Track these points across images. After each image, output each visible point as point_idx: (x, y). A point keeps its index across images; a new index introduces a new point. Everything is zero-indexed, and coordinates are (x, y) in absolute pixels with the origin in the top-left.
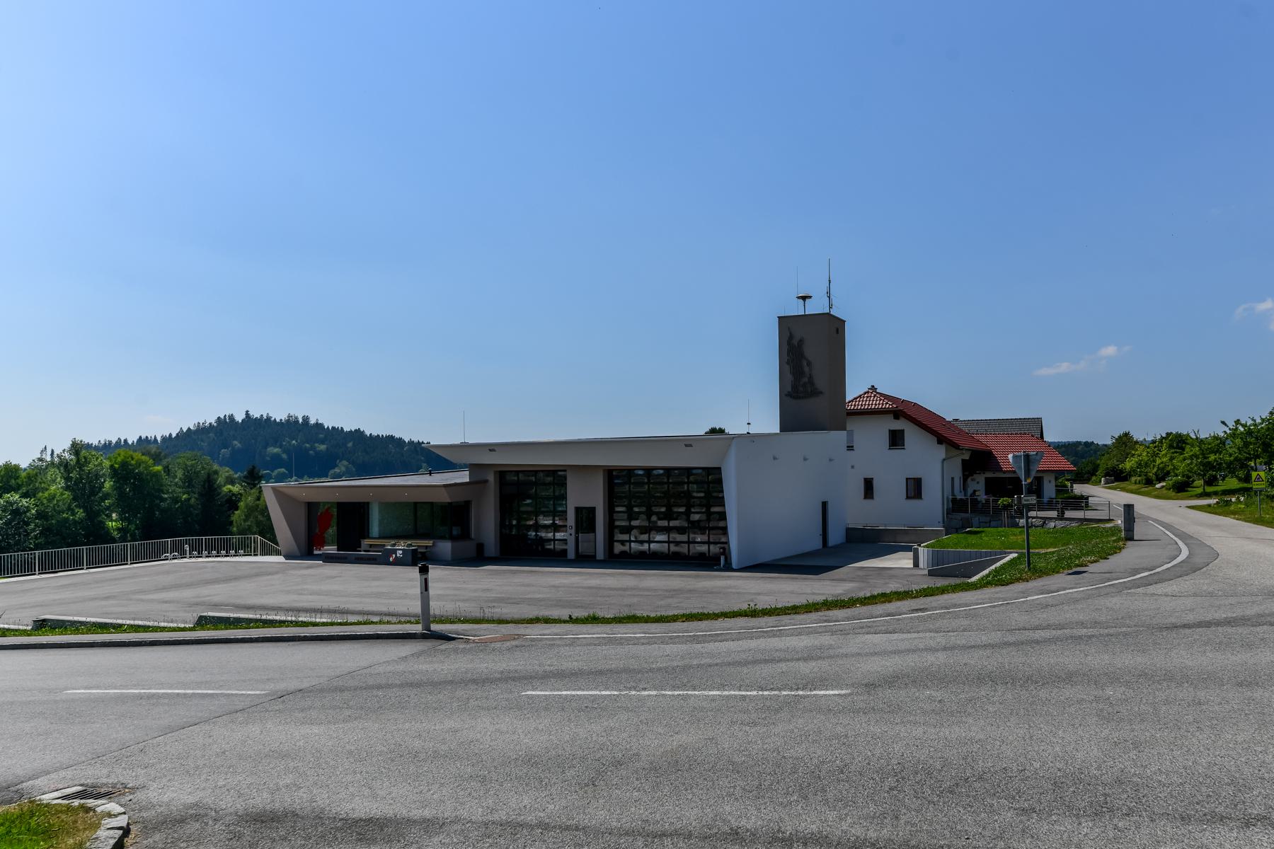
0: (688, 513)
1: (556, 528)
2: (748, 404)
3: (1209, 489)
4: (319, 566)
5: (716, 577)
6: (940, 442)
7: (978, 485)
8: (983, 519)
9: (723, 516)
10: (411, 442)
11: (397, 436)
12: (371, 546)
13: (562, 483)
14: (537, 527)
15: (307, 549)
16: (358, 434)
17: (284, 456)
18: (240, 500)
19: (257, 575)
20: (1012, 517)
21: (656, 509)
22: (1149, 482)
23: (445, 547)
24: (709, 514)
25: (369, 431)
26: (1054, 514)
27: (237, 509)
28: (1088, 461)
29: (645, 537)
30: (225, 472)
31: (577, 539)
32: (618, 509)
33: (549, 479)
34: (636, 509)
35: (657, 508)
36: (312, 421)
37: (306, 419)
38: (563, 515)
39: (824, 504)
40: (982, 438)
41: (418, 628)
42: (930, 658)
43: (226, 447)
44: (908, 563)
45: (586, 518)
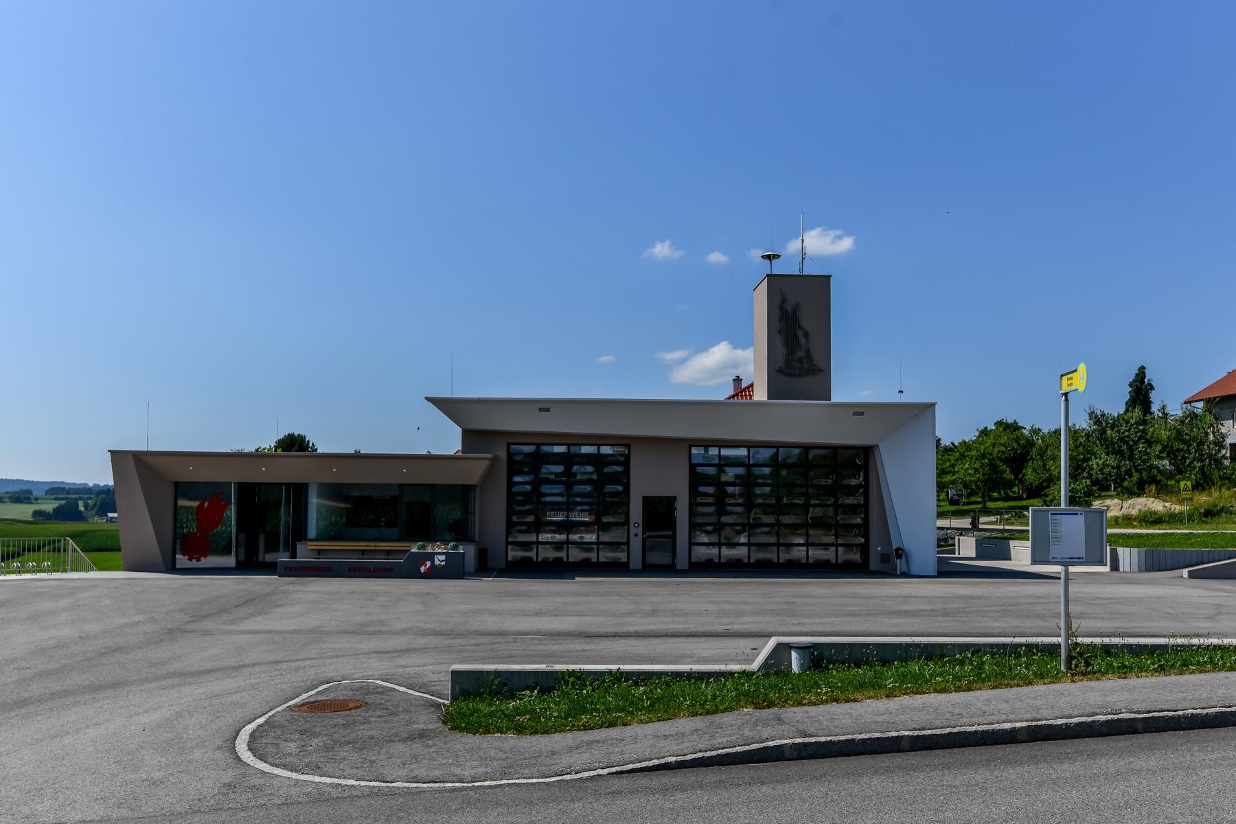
0: (806, 507)
5: (887, 584)
42: (601, 619)
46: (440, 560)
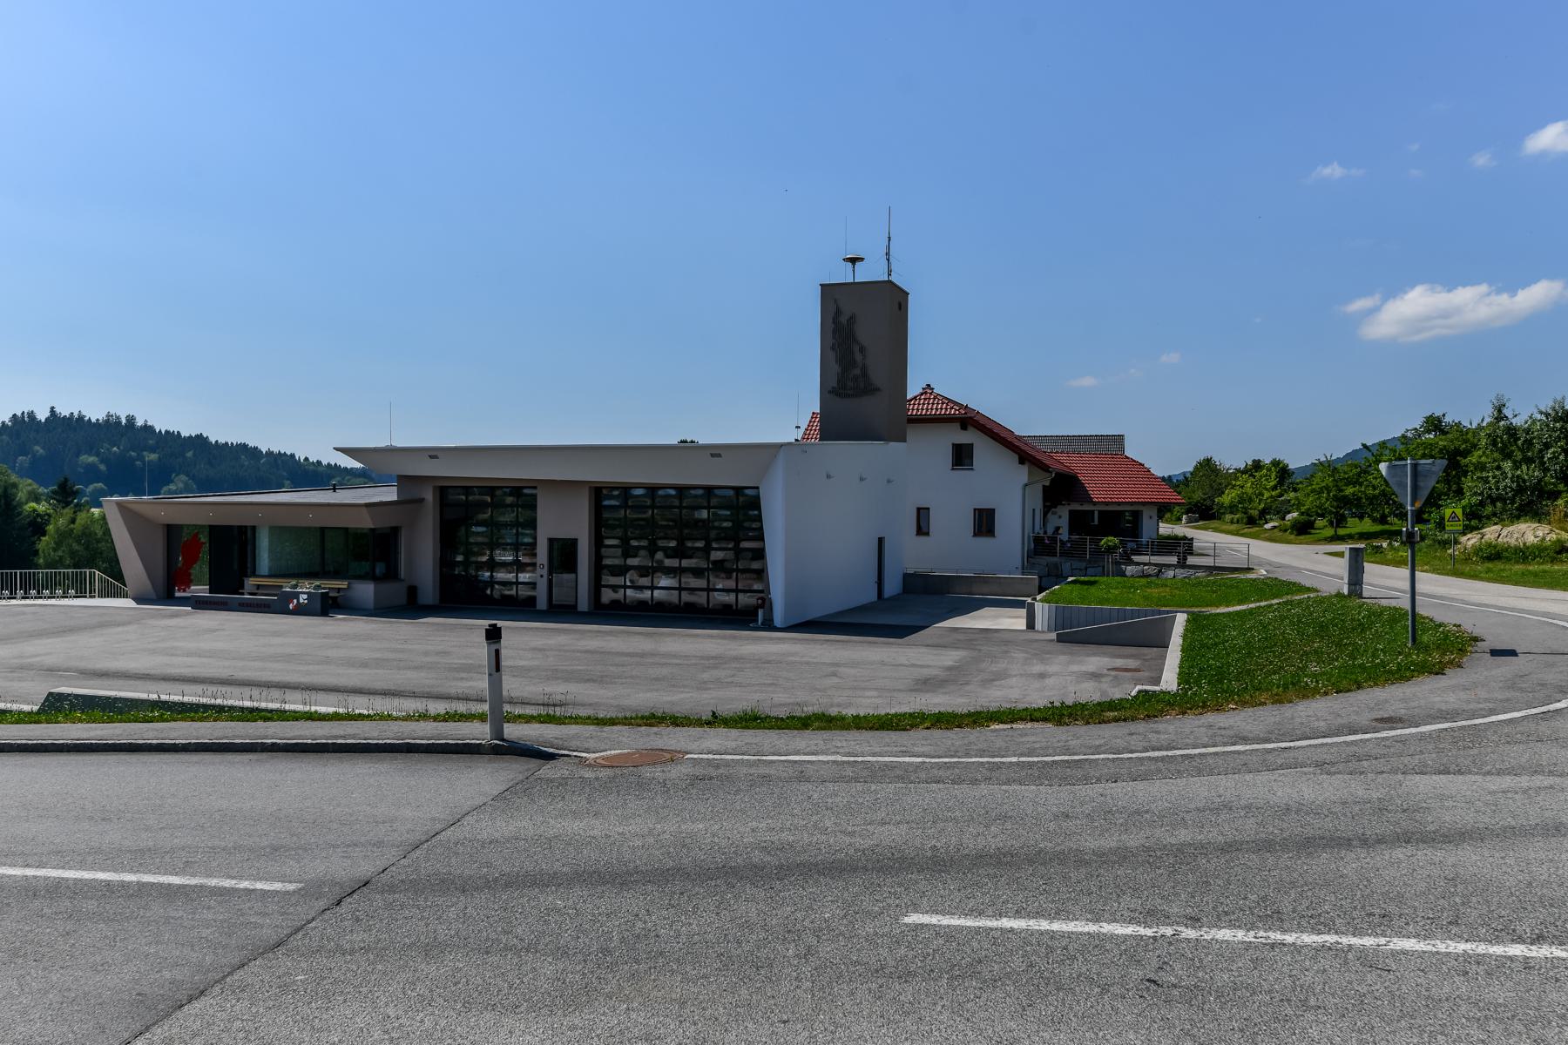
0: (707, 551)
1: (519, 567)
2: (761, 401)
3: (1341, 532)
4: (188, 614)
6: (1022, 462)
7: (1061, 519)
8: (1077, 564)
9: (760, 554)
10: (270, 453)
11: (251, 444)
12: (258, 587)
13: (532, 505)
14: (493, 565)
15: (167, 589)
16: (200, 441)
17: (103, 467)
18: (48, 523)
19: (102, 625)
20: (1118, 563)
21: (661, 543)
22: (1251, 521)
23: (365, 591)
24: (738, 552)
25: (216, 435)
26: (1173, 560)
27: (44, 534)
28: (1206, 494)
29: (645, 581)
30: (25, 486)
31: (550, 582)
32: (608, 542)
33: (509, 500)
34: (634, 543)
35: (671, 542)
36: (140, 423)
37: (131, 419)
38: (532, 549)
39: (881, 540)
40: (1063, 458)
41: (479, 732)
43: (25, 454)
44: (1021, 624)
45: (563, 554)
46: (303, 598)
